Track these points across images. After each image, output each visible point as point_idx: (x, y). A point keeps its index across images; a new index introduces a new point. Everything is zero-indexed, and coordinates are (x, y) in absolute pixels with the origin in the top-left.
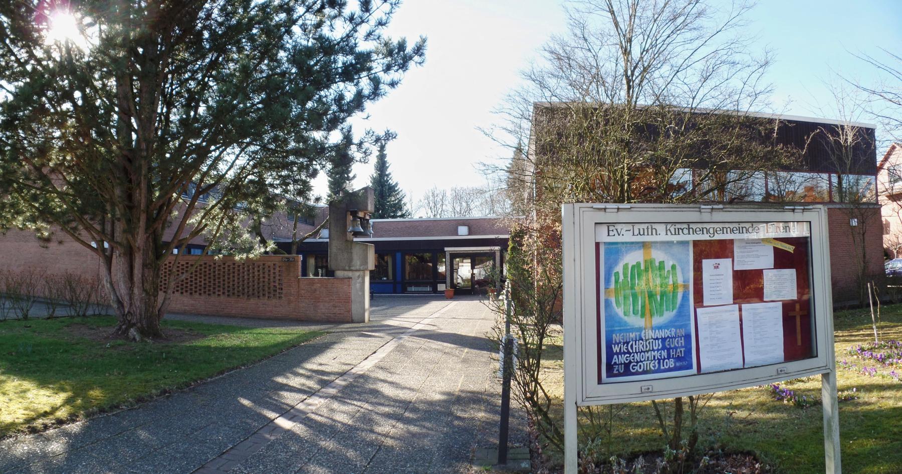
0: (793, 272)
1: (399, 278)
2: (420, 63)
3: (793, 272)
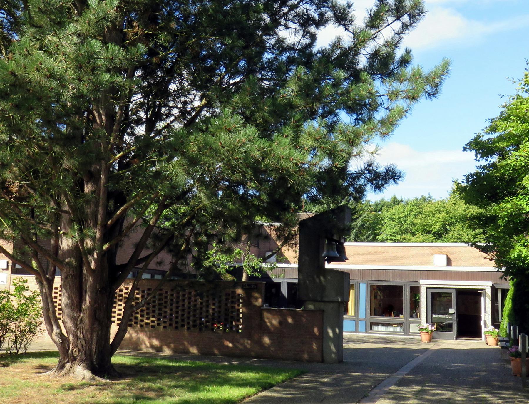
2: (429, 94)
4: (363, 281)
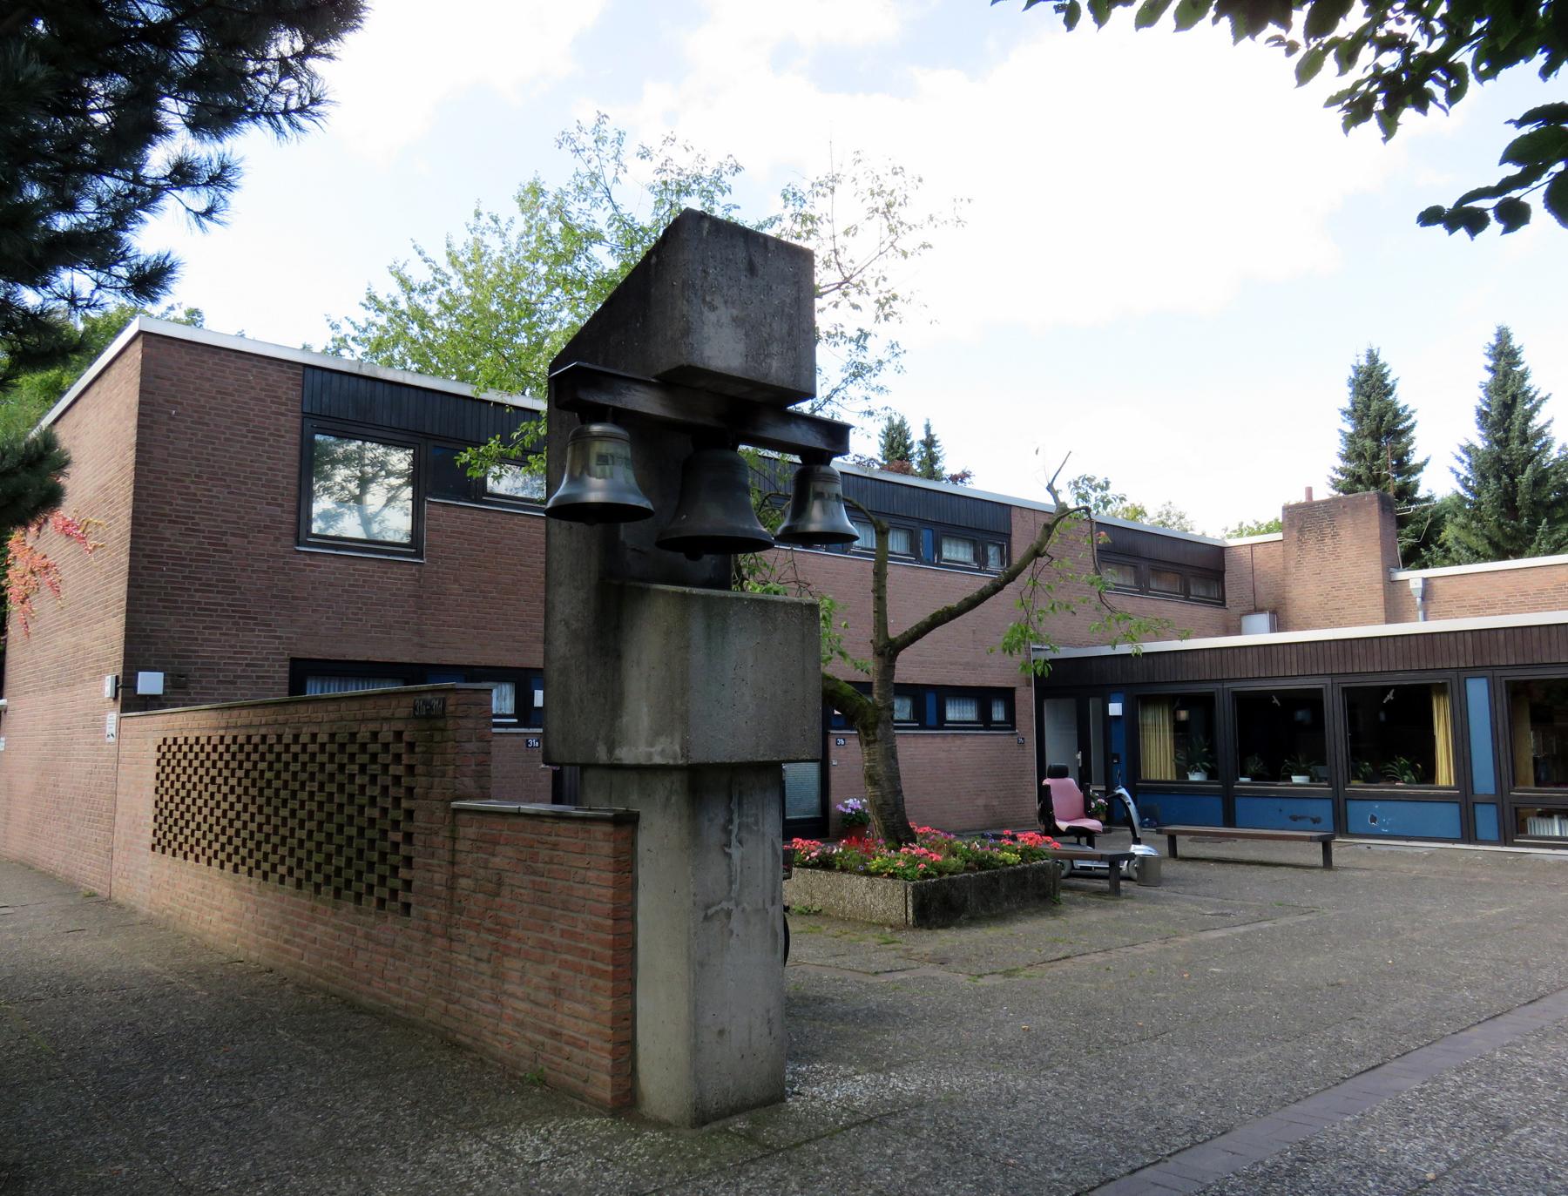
0: (140, 691)
1: (1484, 782)
3: (140, 691)
4: (1475, 671)
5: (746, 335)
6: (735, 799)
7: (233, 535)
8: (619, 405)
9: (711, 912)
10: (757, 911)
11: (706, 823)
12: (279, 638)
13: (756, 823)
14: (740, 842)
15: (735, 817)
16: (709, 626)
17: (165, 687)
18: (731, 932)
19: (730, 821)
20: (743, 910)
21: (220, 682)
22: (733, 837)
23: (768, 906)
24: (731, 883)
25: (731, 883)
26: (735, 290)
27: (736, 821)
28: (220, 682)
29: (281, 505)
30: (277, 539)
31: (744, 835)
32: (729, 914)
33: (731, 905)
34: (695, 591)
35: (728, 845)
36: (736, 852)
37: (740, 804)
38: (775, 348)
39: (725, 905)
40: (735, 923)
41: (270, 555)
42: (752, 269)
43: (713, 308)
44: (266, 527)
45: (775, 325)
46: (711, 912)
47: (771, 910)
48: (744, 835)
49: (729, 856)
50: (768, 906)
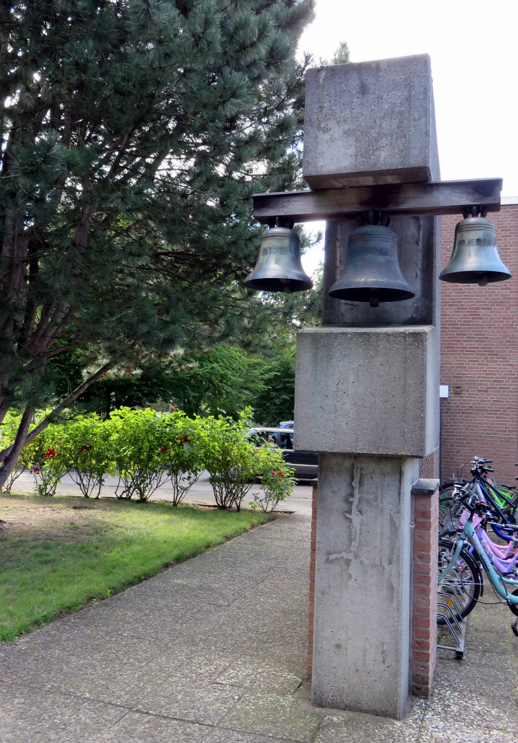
5: (357, 140)
6: (357, 479)
7: (483, 309)
8: (282, 214)
9: (332, 557)
10: (374, 566)
11: (330, 494)
12: (512, 365)
13: (376, 499)
14: (360, 512)
15: (356, 492)
16: (315, 355)
17: (450, 393)
18: (350, 576)
19: (352, 495)
20: (362, 562)
21: (478, 391)
22: (354, 507)
23: (385, 563)
24: (350, 540)
25: (350, 540)
26: (348, 111)
27: (357, 495)
28: (478, 391)
29: (508, 289)
30: (508, 308)
31: (364, 506)
32: (348, 562)
33: (350, 556)
34: (401, 329)
35: (350, 512)
36: (356, 518)
37: (361, 483)
38: (384, 142)
39: (345, 555)
40: (354, 570)
41: (504, 318)
42: (363, 90)
43: (326, 130)
44: (501, 302)
45: (384, 125)
46: (332, 557)
47: (387, 568)
48: (364, 506)
49: (350, 520)
50: (385, 563)
